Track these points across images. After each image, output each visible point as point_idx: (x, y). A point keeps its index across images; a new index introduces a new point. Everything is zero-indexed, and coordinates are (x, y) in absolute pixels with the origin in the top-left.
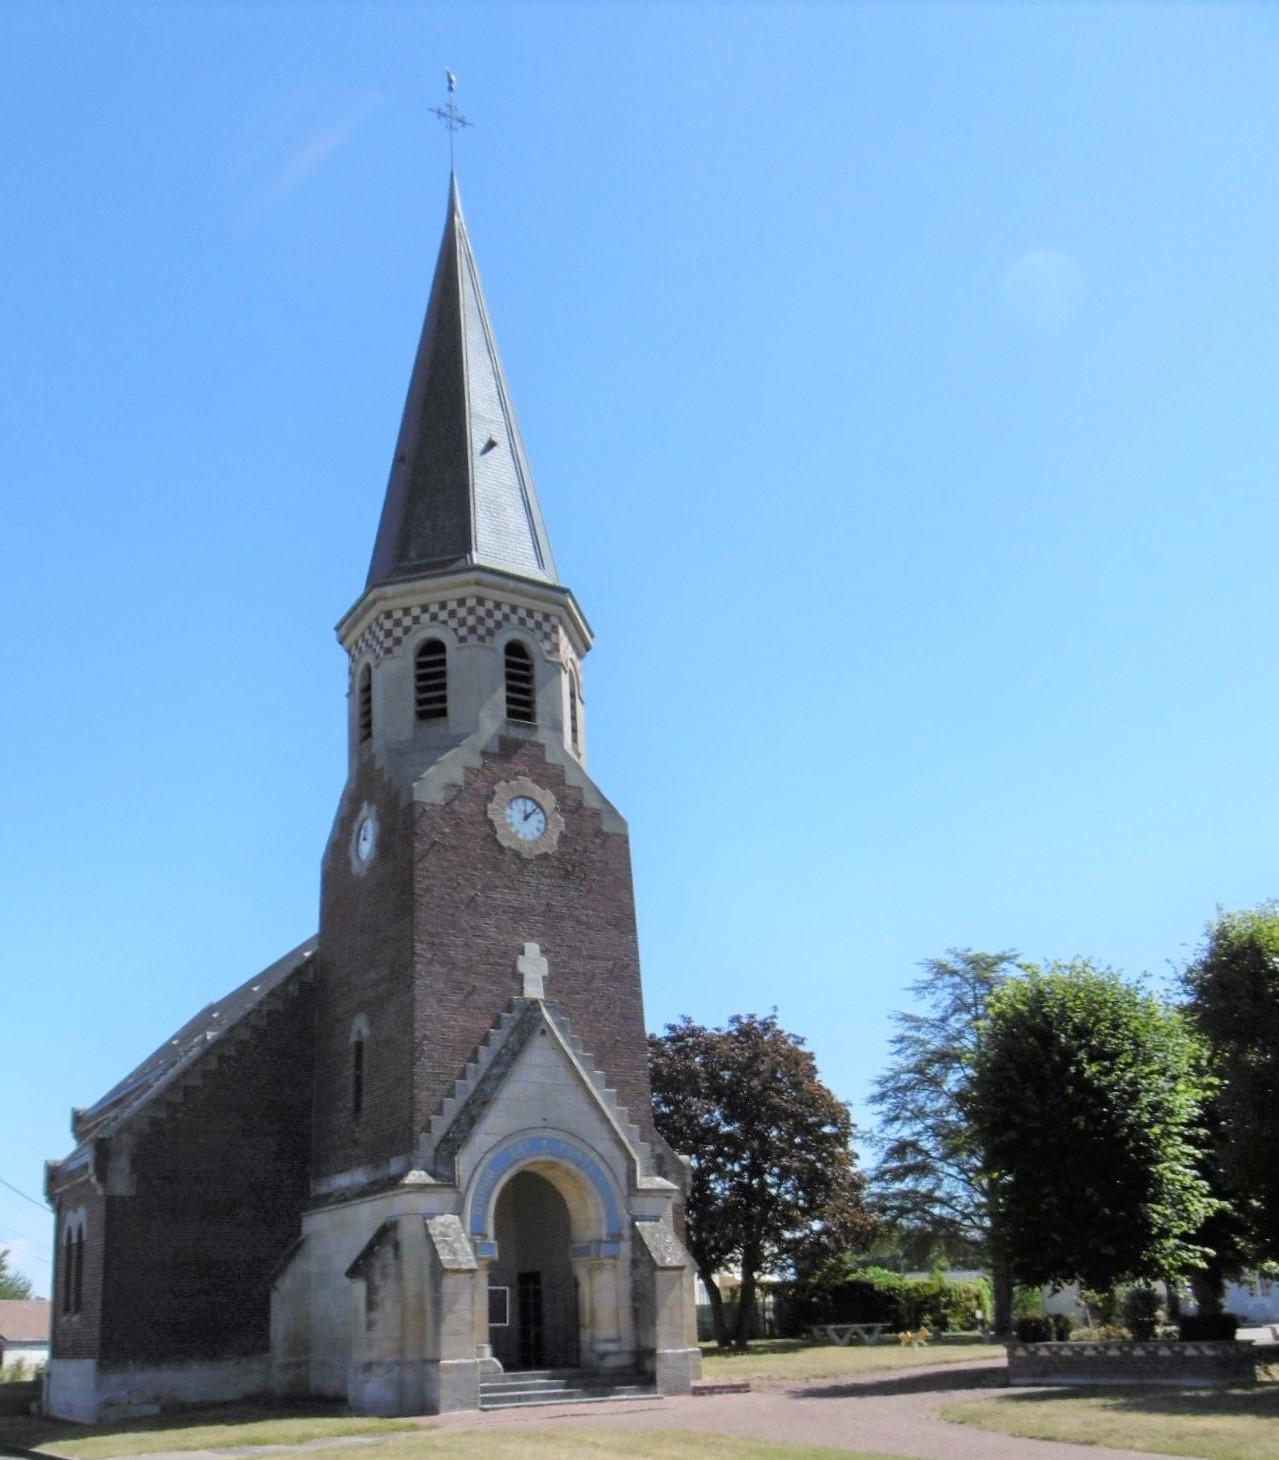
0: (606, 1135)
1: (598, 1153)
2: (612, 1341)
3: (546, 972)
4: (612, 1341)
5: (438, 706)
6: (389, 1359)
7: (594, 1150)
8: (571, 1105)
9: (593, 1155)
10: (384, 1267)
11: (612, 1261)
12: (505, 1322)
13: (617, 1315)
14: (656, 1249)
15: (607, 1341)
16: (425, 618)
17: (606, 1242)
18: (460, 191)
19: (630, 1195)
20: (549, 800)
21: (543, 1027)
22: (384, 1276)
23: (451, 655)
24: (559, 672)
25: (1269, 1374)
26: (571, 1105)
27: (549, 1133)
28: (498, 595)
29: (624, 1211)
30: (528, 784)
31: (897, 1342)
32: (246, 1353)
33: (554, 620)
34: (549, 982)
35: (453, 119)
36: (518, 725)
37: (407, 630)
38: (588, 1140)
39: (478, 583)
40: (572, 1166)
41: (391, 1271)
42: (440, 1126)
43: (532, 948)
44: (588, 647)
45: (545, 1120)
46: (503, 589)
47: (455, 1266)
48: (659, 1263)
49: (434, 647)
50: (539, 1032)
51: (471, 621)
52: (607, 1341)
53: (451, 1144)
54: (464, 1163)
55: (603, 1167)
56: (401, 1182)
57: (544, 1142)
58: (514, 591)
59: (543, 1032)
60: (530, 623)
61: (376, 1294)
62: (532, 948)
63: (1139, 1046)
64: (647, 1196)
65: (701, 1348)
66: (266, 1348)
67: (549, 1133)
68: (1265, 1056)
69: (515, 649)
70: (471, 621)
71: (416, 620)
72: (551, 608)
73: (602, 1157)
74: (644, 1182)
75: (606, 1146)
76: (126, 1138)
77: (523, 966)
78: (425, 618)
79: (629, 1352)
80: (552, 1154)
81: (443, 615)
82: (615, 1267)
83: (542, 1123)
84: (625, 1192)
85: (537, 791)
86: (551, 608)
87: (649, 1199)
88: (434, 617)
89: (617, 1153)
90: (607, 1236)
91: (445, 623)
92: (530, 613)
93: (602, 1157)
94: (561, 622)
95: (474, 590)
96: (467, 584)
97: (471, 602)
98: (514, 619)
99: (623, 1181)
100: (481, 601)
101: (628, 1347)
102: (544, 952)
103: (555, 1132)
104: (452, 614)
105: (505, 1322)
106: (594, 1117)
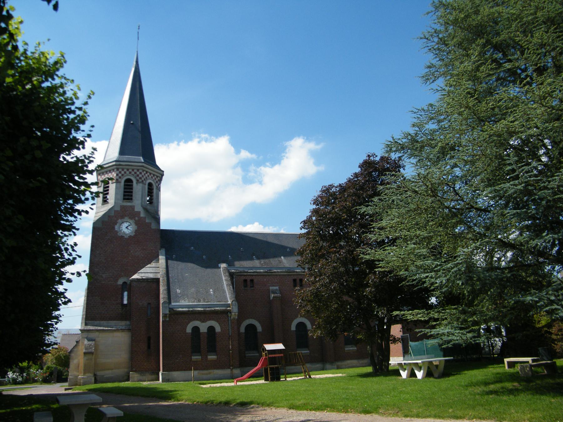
5: (126, 190)
12: (508, 362)
16: (128, 172)
25: (67, 298)
31: (460, 374)
37: (123, 175)
56: (163, 251)
60: (133, 173)
63: (533, 411)
68: (54, 296)
69: (150, 185)
71: (125, 173)
78: (128, 172)
81: (133, 173)
88: (130, 173)
91: (133, 175)
92: (133, 170)
97: (140, 171)
98: (150, 176)
104: (135, 173)
105: (508, 362)
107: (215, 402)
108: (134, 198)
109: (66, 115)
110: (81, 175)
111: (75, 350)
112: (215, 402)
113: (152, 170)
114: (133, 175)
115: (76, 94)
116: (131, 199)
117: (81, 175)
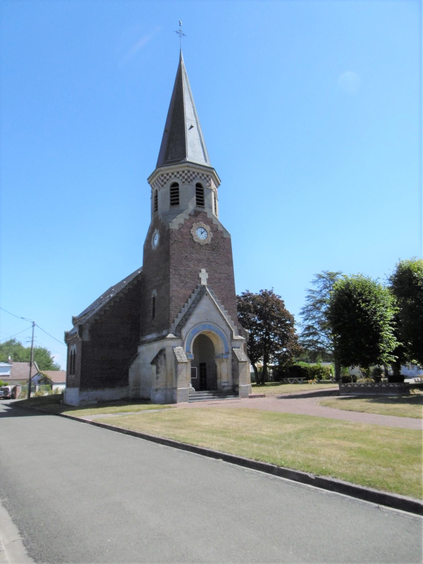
0: (225, 324)
1: (222, 329)
2: (226, 382)
3: (207, 277)
4: (226, 382)
6: (163, 388)
7: (221, 328)
8: (215, 315)
9: (221, 329)
10: (161, 362)
11: (226, 360)
13: (228, 375)
14: (239, 356)
15: (225, 382)
16: (173, 176)
17: (225, 354)
18: (183, 55)
19: (231, 341)
20: (208, 228)
21: (207, 293)
22: (161, 364)
23: (181, 187)
24: (211, 192)
26: (215, 315)
27: (208, 323)
28: (194, 170)
29: (230, 346)
30: (202, 224)
32: (122, 386)
33: (210, 177)
34: (208, 280)
35: (180, 34)
36: (199, 207)
37: (168, 180)
38: (219, 325)
39: (188, 166)
40: (215, 333)
41: (163, 362)
42: (177, 321)
43: (203, 270)
44: (219, 185)
45: (207, 319)
46: (195, 168)
47: (181, 361)
48: (240, 360)
49: (175, 185)
50: (205, 294)
51: (186, 177)
52: (225, 382)
53: (180, 326)
54: (184, 332)
55: (223, 333)
57: (207, 326)
58: (198, 169)
59: (207, 294)
60: (203, 178)
61: (159, 369)
62: (203, 270)
64: (236, 341)
65: (251, 384)
66: (127, 385)
67: (208, 323)
69: (199, 185)
70: (186, 177)
71: (170, 177)
72: (209, 174)
73: (223, 330)
74: (235, 337)
75: (224, 327)
76: (88, 325)
77: (201, 275)
78: (173, 176)
79: (231, 386)
80: (209, 329)
81: (178, 176)
82: (227, 361)
83: (206, 321)
84: (230, 340)
85: (205, 226)
86: (209, 174)
87: (237, 342)
88: (175, 176)
89: (228, 329)
90: (225, 352)
91: (178, 178)
92: (203, 175)
93: (223, 330)
94: (212, 177)
95: (187, 168)
96: (185, 167)
98: (198, 177)
99: (229, 337)
101: (231, 384)
102: (207, 271)
103: (210, 323)
104: (181, 175)
106: (221, 319)
107: (340, 277)
108: (180, 201)
109: (372, 321)
110: (379, 365)
111: (360, 411)
112: (340, 277)
113: (204, 171)
114: (178, 178)
115: (191, 308)
116: (178, 203)
117: (379, 365)
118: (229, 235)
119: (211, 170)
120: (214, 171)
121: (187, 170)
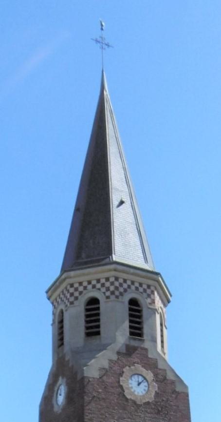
28: (125, 276)
33: (152, 288)
39: (115, 270)
44: (169, 301)
46: (128, 273)
49: (94, 301)
58: (133, 274)
72: (150, 282)
86: (150, 282)
91: (99, 289)
94: (156, 289)
95: (113, 273)
96: (110, 270)
98: (133, 287)
100: (117, 279)
118: (186, 387)
119: (155, 276)
120: (160, 279)
121: (113, 276)
